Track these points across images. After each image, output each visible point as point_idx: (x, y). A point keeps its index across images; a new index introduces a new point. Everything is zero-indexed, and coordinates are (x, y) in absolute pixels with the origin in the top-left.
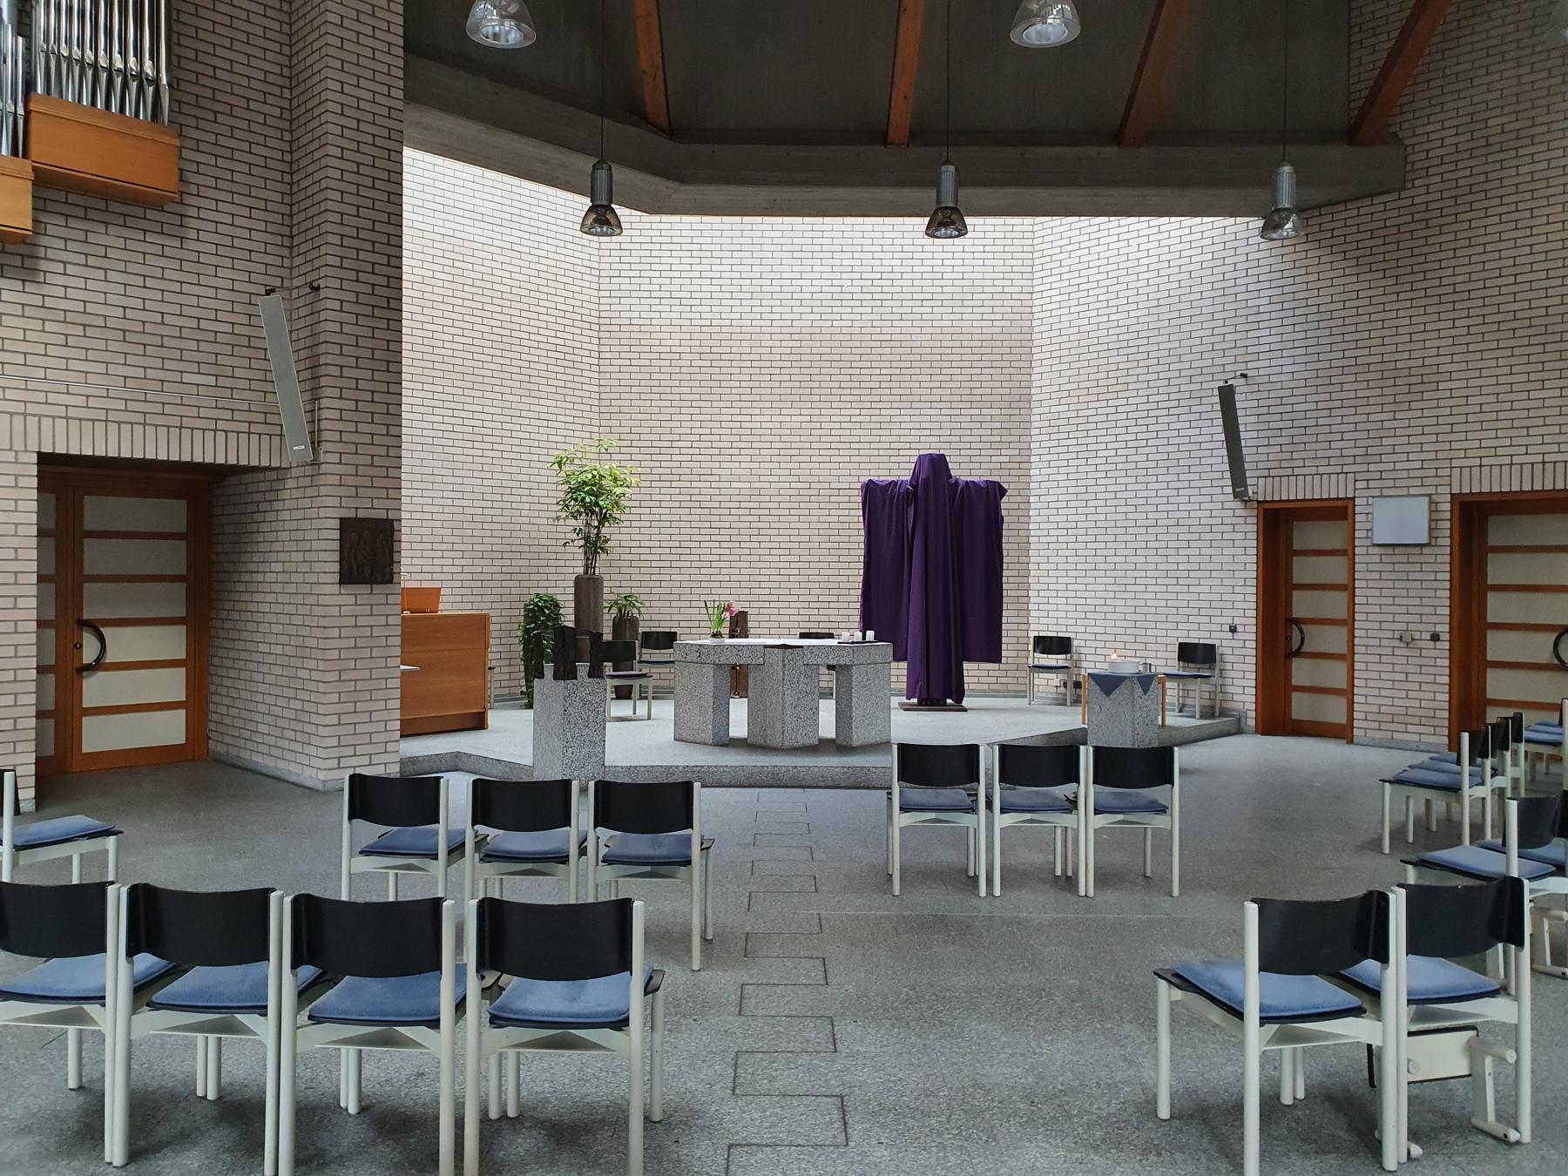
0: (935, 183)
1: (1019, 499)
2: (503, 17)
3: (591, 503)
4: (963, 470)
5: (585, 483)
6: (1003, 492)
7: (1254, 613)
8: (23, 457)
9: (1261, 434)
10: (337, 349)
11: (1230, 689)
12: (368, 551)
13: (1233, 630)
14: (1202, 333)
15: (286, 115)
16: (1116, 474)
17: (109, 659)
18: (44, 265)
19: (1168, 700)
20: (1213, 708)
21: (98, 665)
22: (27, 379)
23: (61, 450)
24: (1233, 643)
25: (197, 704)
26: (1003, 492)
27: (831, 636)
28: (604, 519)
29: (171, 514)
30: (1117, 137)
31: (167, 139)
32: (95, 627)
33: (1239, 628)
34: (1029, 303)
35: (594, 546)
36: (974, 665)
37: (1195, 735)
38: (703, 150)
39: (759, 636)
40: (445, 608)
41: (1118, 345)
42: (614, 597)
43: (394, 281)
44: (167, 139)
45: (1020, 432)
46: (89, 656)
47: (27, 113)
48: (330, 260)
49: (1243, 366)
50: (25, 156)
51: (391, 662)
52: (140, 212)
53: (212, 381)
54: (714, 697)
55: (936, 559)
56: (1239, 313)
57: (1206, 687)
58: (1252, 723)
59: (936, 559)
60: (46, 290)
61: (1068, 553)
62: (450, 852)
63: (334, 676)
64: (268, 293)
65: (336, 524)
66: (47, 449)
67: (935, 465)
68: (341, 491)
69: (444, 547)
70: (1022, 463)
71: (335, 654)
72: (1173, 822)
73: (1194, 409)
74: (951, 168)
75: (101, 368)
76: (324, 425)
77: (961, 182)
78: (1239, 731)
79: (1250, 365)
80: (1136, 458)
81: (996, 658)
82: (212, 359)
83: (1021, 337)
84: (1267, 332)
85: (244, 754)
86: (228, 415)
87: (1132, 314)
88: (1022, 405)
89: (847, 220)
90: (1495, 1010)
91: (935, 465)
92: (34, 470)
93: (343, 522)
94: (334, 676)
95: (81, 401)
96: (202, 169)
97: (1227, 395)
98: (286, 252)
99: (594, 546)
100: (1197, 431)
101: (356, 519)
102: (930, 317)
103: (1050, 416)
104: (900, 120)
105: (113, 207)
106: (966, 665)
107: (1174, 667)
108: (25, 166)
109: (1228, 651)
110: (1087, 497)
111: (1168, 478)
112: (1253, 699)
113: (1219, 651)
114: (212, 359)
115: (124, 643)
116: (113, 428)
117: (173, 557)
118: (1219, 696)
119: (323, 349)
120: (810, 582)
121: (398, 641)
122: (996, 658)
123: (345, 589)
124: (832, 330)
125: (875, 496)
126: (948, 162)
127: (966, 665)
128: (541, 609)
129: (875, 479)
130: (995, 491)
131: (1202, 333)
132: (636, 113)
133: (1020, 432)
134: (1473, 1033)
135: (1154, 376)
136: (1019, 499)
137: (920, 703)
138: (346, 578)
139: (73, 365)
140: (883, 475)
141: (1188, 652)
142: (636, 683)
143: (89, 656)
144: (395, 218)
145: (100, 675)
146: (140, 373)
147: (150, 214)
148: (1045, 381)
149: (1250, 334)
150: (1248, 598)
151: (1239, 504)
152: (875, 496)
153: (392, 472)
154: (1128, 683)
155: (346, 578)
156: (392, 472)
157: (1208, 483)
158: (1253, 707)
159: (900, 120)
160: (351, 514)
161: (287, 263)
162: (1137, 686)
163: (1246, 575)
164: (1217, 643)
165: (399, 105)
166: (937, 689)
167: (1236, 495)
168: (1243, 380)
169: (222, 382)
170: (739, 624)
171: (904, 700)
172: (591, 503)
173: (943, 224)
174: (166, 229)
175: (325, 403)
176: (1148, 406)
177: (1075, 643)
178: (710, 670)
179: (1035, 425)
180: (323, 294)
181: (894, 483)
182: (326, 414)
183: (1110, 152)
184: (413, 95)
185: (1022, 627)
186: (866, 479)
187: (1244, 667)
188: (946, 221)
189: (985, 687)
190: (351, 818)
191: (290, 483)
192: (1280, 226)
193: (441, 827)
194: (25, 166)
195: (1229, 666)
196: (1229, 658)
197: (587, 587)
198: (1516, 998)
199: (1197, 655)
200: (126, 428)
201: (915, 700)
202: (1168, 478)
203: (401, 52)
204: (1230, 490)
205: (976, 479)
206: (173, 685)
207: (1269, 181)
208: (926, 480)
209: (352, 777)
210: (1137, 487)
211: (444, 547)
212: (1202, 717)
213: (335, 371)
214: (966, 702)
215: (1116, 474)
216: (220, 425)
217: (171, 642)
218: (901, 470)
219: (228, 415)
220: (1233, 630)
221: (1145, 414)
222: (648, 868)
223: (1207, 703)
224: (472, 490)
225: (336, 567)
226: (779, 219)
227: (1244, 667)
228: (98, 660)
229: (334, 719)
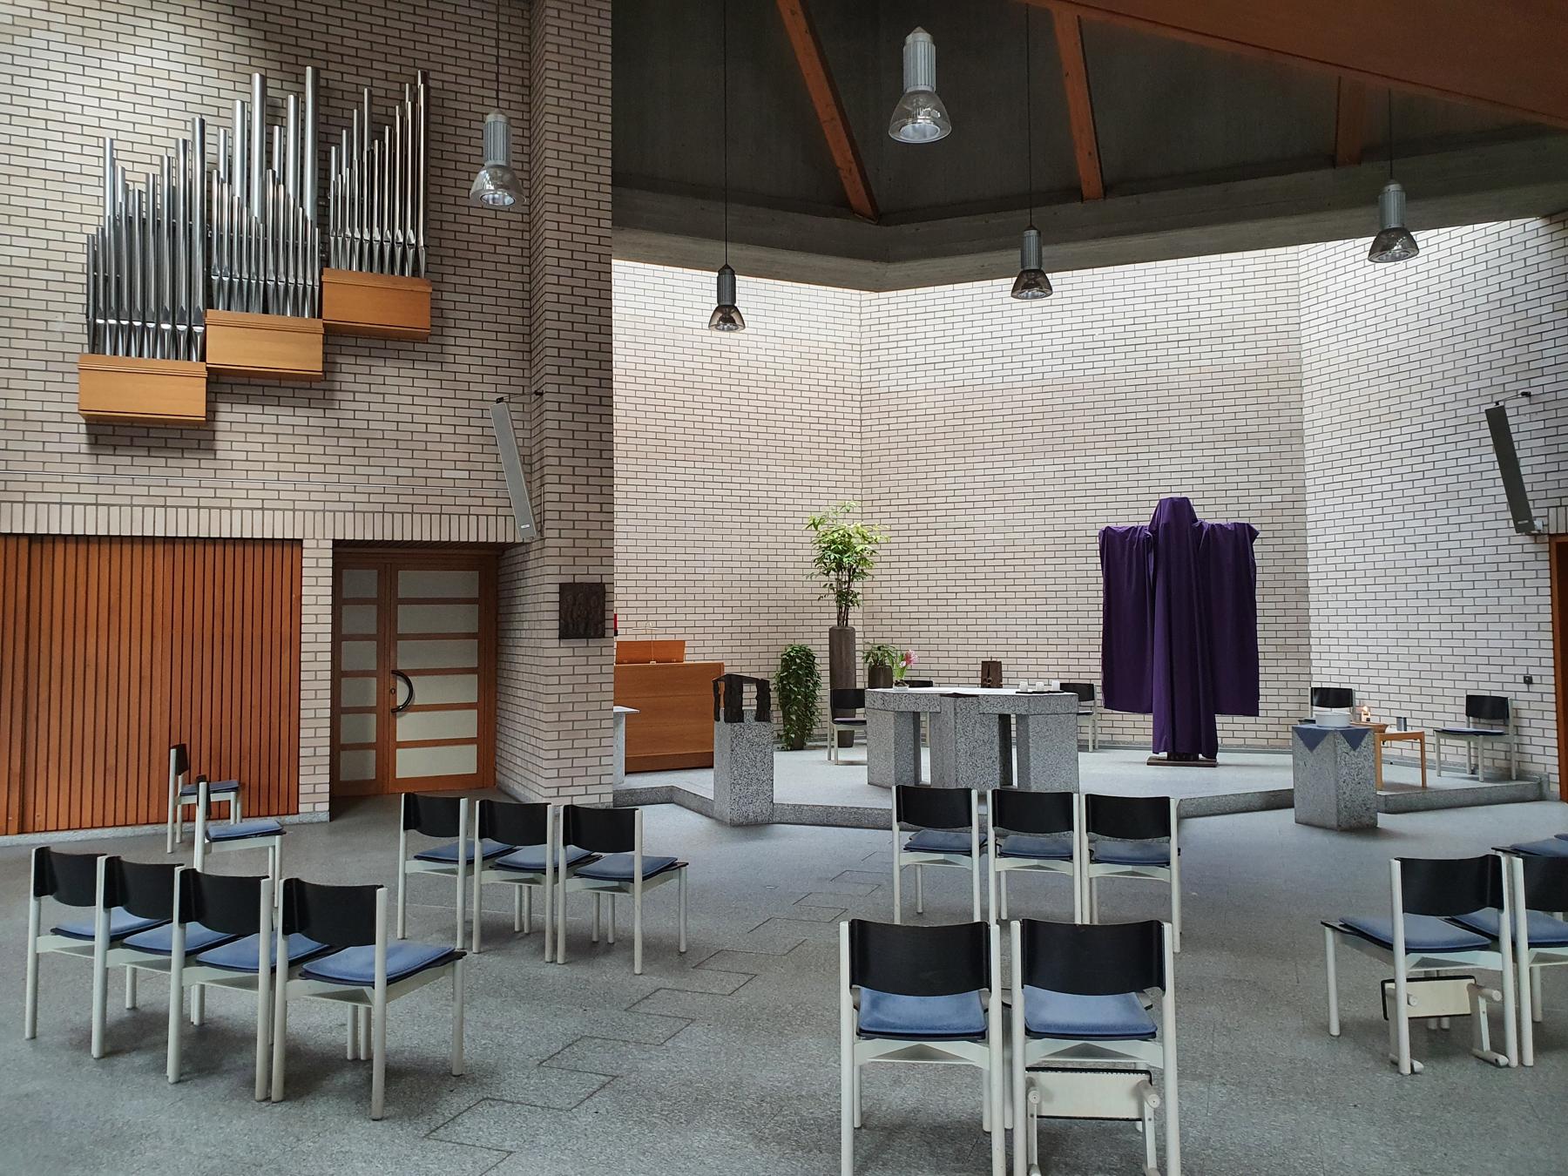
0: (1020, 244)
1: (1295, 541)
2: (497, 187)
3: (842, 560)
4: (1208, 513)
5: (833, 542)
6: (1253, 534)
7: (1551, 662)
8: (323, 544)
9: (1549, 459)
10: (556, 443)
11: (1529, 749)
12: (585, 611)
13: (1528, 681)
14: (1478, 351)
15: (526, 253)
16: (1393, 510)
17: (417, 701)
18: (339, 396)
19: (1428, 756)
20: (1509, 770)
21: (406, 707)
22: (325, 484)
23: (349, 537)
24: (1528, 696)
25: (489, 740)
26: (1253, 534)
27: (929, 684)
28: (853, 573)
29: (463, 583)
30: (1332, 161)
31: (421, 288)
32: (404, 675)
33: (1535, 680)
34: (1297, 334)
35: (845, 598)
36: (1228, 719)
37: (1470, 798)
38: (908, 229)
39: (939, 685)
40: (691, 657)
41: (1389, 371)
42: (869, 648)
43: (606, 381)
44: (421, 288)
45: (1293, 469)
46: (401, 700)
47: (321, 283)
48: (549, 369)
49: (1525, 384)
50: (320, 316)
51: (605, 705)
52: (410, 346)
53: (465, 474)
54: (896, 743)
55: (1185, 610)
56: (1519, 325)
57: (1499, 746)
58: (1556, 788)
59: (1185, 610)
60: (339, 414)
61: (1347, 597)
62: (644, 879)
63: (554, 717)
64: (500, 400)
65: (556, 588)
66: (339, 537)
67: (1178, 510)
68: (561, 561)
69: (715, 604)
70: (1297, 500)
71: (555, 699)
72: (1172, 875)
73: (1473, 435)
74: (1033, 232)
75: (380, 471)
76: (548, 506)
77: (1043, 241)
78: (1541, 798)
79: (1534, 382)
80: (1413, 492)
81: (1252, 710)
82: (465, 456)
83: (1288, 370)
84: (1551, 343)
85: (511, 784)
86: (479, 502)
87: (1402, 337)
88: (1294, 441)
89: (920, 290)
90: (1143, 1053)
91: (1178, 510)
92: (330, 553)
93: (563, 588)
94: (554, 717)
95: (364, 498)
96: (459, 306)
97: (1497, 419)
98: (526, 365)
99: (845, 598)
100: (1477, 459)
101: (574, 584)
102: (1187, 357)
103: (1323, 451)
104: (1088, 174)
105: (389, 344)
106: (1219, 718)
107: (1462, 723)
108: (319, 324)
109: (1524, 705)
110: (1364, 535)
111: (1448, 512)
112: (1556, 761)
113: (1512, 705)
114: (465, 456)
115: (426, 690)
116: (388, 517)
117: (465, 619)
118: (1516, 757)
119: (545, 443)
120: (1057, 631)
121: (611, 687)
122: (1252, 710)
123: (564, 643)
124: (1085, 379)
125: (1113, 544)
126: (1031, 227)
127: (1219, 718)
128: (793, 659)
129: (1113, 525)
130: (1245, 534)
131: (1478, 351)
132: (841, 206)
133: (1293, 469)
134: (1144, 1077)
135: (1429, 402)
136: (1295, 541)
137: (1169, 758)
138: (564, 634)
139: (359, 470)
140: (1122, 522)
141: (1476, 706)
142: (858, 730)
143: (401, 700)
144: (606, 329)
145: (410, 715)
146: (409, 472)
147: (418, 347)
148: (1317, 414)
149: (1532, 348)
150: (1544, 645)
151: (1527, 539)
152: (1113, 544)
153: (606, 543)
154: (1330, 737)
155: (564, 634)
156: (606, 543)
157: (1492, 517)
158: (1556, 770)
159: (1088, 174)
160: (569, 580)
161: (527, 374)
162: (1344, 746)
163: (1539, 618)
164: (1510, 696)
165: (608, 233)
166: (1188, 742)
167: (1519, 529)
168: (1525, 400)
169: (474, 475)
170: (991, 673)
171: (1150, 754)
172: (842, 560)
173: (1027, 287)
174: (430, 357)
175: (548, 488)
176: (1424, 435)
177: (1357, 695)
178: (891, 716)
179: (1308, 461)
180: (545, 397)
181: (1134, 529)
182: (548, 497)
183: (1324, 176)
184: (619, 222)
185: (1303, 678)
186: (1103, 527)
187: (1544, 724)
188: (1031, 282)
189: (1264, 742)
190: (481, 837)
191: (532, 555)
192: (1388, 248)
193: (636, 854)
194: (319, 324)
195: (1525, 723)
196: (1523, 714)
197: (841, 638)
198: (1162, 1041)
199: (1488, 710)
200: (388, 517)
201: (1164, 755)
202: (1448, 512)
203: (609, 189)
204: (1512, 524)
205: (1223, 522)
206: (466, 723)
207: (1373, 199)
208: (1166, 526)
209: (566, 807)
210: (1415, 524)
211: (715, 604)
212: (1486, 780)
213: (555, 461)
214: (1220, 757)
215: (1393, 510)
216: (473, 510)
217: (466, 689)
218: (1138, 515)
219: (479, 502)
220: (1528, 681)
221: (1419, 444)
222: (616, 884)
223: (1503, 764)
224: (694, 557)
225: (556, 625)
226: (931, 289)
227: (1544, 724)
228: (405, 705)
229: (554, 755)
